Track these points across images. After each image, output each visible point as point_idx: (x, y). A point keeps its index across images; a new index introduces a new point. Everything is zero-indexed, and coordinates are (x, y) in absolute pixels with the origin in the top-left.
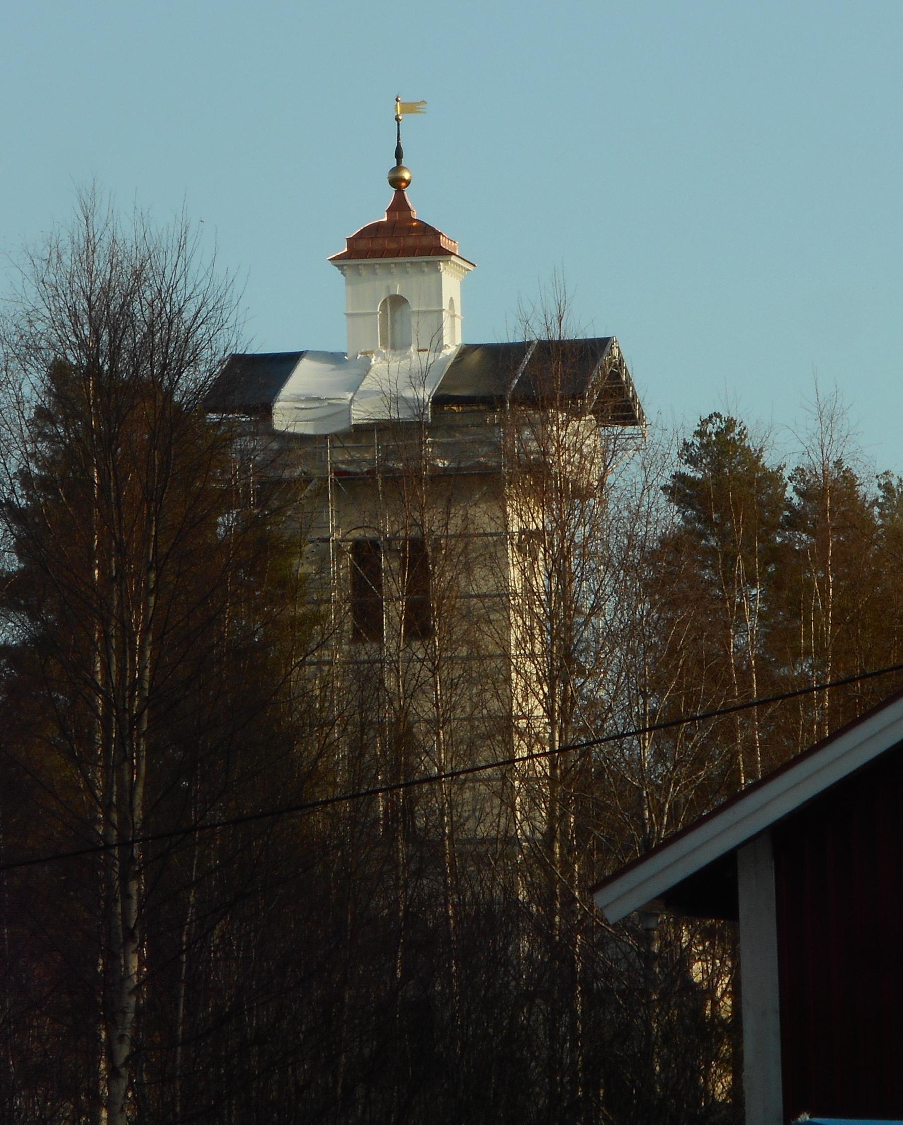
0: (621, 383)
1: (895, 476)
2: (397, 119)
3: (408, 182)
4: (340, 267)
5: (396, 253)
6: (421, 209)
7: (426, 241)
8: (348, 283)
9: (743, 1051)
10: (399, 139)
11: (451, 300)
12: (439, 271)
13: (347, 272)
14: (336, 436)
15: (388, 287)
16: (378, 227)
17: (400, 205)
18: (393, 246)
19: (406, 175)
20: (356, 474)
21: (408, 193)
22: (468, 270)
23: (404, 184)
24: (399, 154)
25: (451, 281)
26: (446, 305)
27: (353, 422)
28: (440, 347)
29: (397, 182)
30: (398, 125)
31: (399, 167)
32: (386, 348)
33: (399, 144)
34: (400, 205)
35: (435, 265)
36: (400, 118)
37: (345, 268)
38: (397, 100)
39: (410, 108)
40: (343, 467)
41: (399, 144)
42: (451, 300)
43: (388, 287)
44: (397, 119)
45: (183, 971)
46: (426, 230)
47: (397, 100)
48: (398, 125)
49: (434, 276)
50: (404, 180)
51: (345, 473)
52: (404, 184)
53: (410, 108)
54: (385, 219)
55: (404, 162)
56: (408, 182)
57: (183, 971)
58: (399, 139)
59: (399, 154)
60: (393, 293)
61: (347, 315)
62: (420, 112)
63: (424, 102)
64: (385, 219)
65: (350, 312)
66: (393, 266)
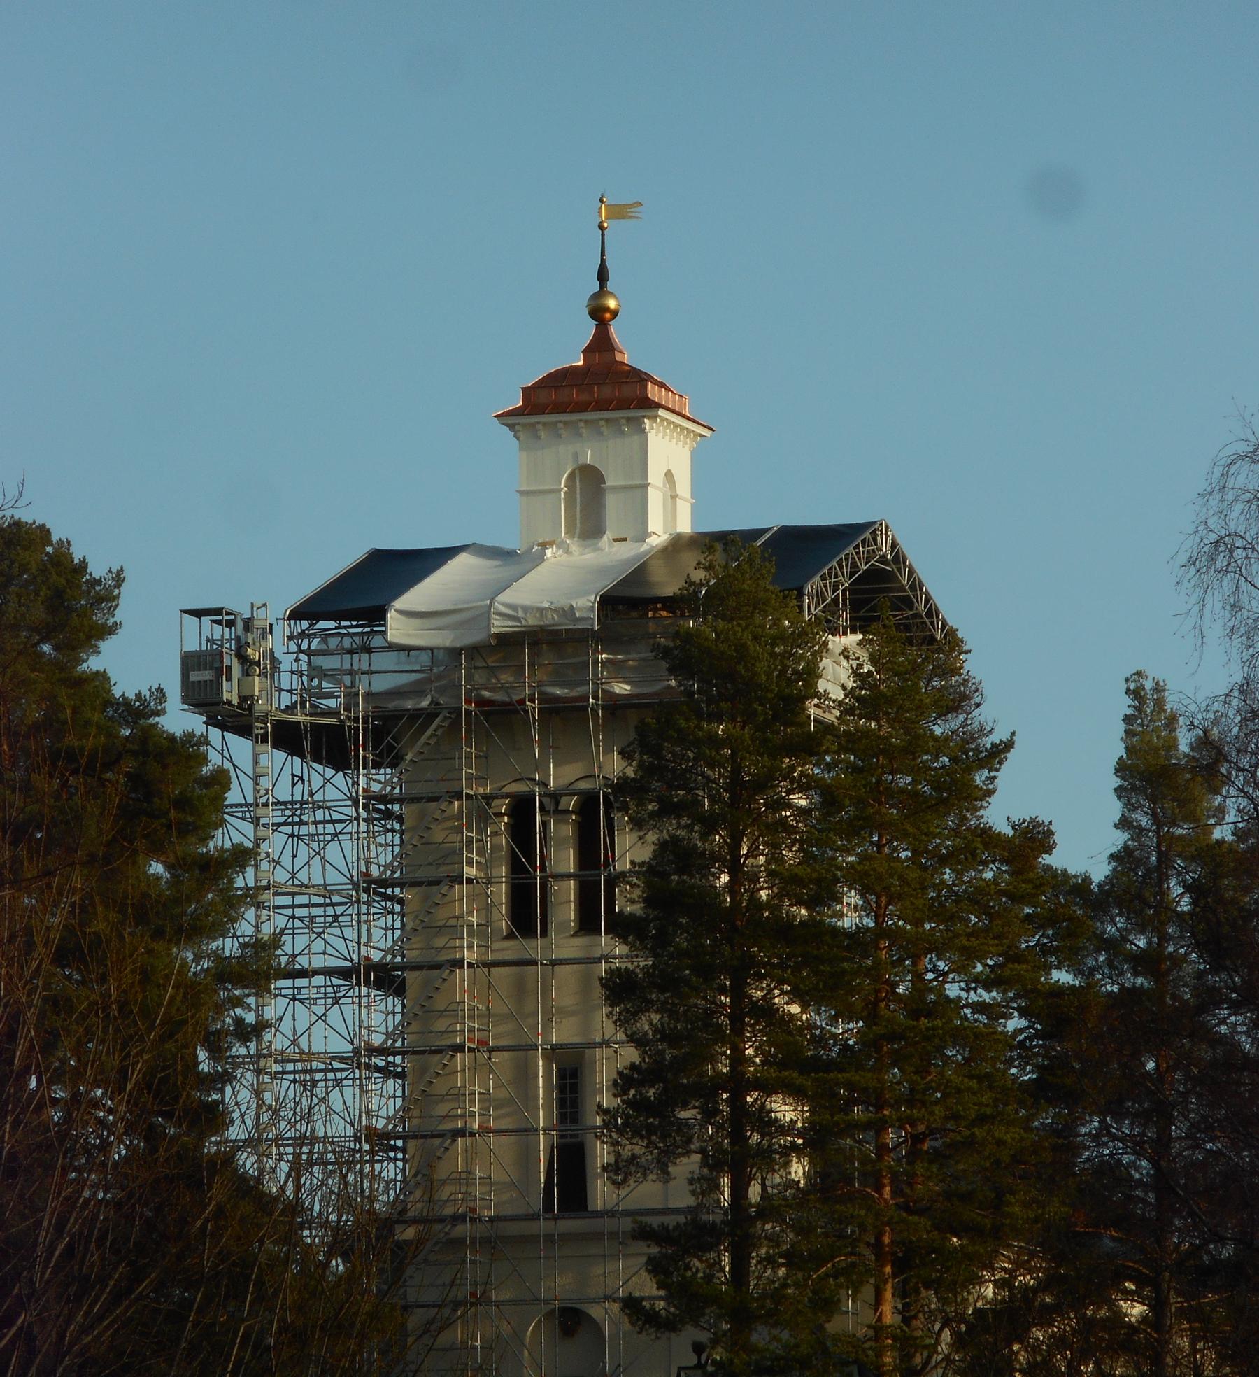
0: (903, 589)
1: (1150, 679)
2: (601, 227)
3: (615, 314)
4: (512, 427)
5: (581, 408)
6: (630, 352)
7: (627, 391)
8: (521, 449)
10: (603, 254)
11: (669, 475)
12: (643, 431)
13: (521, 434)
14: (474, 651)
15: (576, 455)
17: (601, 344)
18: (584, 397)
19: (612, 304)
20: (503, 704)
21: (614, 329)
22: (701, 436)
23: (608, 315)
24: (602, 275)
25: (667, 451)
26: (655, 476)
27: (493, 630)
28: (644, 535)
29: (599, 314)
30: (603, 235)
31: (603, 292)
32: (572, 537)
33: (603, 261)
34: (601, 344)
37: (517, 427)
38: (601, 201)
39: (619, 212)
40: (486, 694)
41: (603, 261)
42: (669, 475)
43: (576, 455)
44: (601, 227)
45: (57, 1253)
46: (641, 378)
47: (601, 201)
48: (603, 235)
50: (607, 309)
51: (489, 703)
52: (608, 315)
53: (619, 212)
54: (581, 363)
55: (610, 286)
56: (615, 314)
57: (57, 1253)
58: (603, 254)
59: (602, 275)
60: (581, 462)
61: (521, 493)
62: (631, 217)
63: (640, 204)
64: (581, 363)
65: (524, 488)
66: (582, 424)
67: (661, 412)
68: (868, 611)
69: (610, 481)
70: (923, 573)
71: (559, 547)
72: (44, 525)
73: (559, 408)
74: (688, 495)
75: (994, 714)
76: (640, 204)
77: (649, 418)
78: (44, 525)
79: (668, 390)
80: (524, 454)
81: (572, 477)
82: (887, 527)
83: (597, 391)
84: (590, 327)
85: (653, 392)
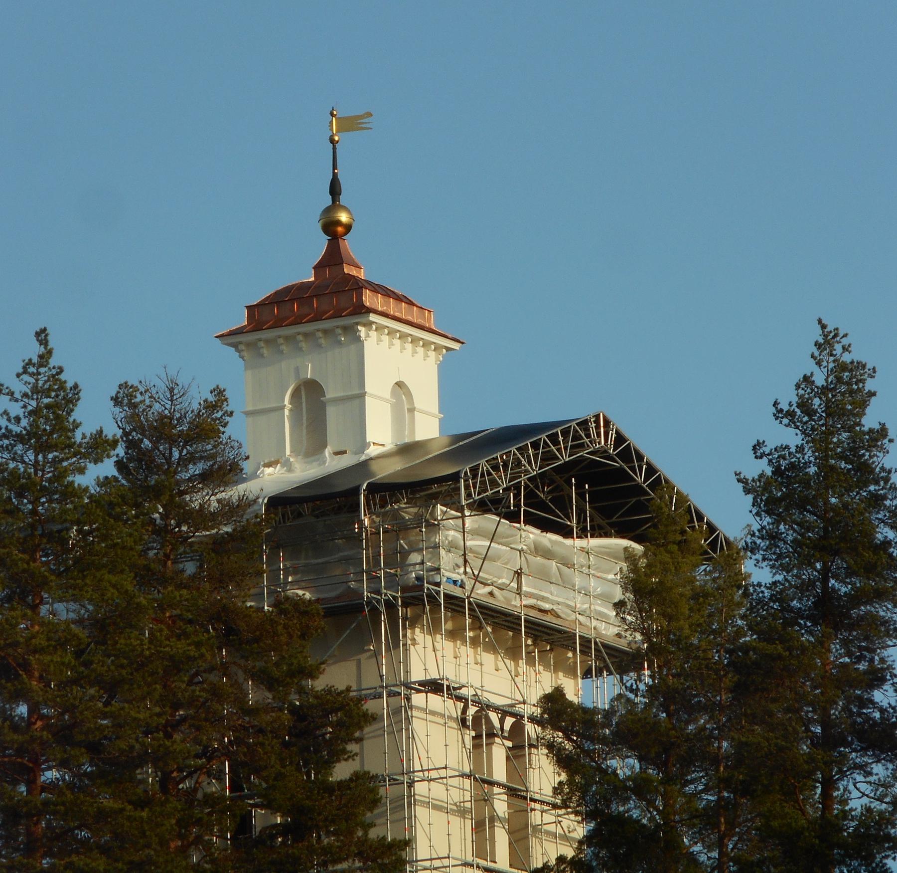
2: (332, 141)
3: (348, 228)
4: (235, 346)
8: (246, 368)
9: (682, 499)
12: (358, 339)
13: (245, 354)
15: (297, 370)
16: (302, 287)
17: (334, 257)
19: (344, 217)
21: (349, 244)
22: (448, 349)
24: (335, 189)
29: (331, 228)
30: (334, 149)
32: (297, 455)
33: (335, 176)
34: (334, 257)
35: (351, 331)
36: (336, 138)
37: (241, 347)
38: (332, 115)
39: (350, 124)
41: (335, 176)
43: (297, 370)
44: (332, 141)
47: (332, 115)
48: (334, 149)
49: (353, 347)
50: (339, 223)
52: (340, 229)
53: (350, 124)
54: (312, 279)
55: (343, 199)
56: (348, 228)
59: (335, 189)
60: (302, 376)
63: (369, 115)
64: (312, 279)
65: (250, 408)
67: (373, 317)
68: (622, 516)
69: (330, 394)
70: (667, 469)
71: (283, 466)
72: (102, 461)
73: (278, 323)
74: (434, 408)
75: (685, 494)
76: (369, 115)
77: (364, 325)
78: (102, 461)
79: (411, 303)
80: (249, 372)
81: (296, 395)
82: (607, 423)
83: (324, 302)
84: (323, 242)
85: (368, 298)
